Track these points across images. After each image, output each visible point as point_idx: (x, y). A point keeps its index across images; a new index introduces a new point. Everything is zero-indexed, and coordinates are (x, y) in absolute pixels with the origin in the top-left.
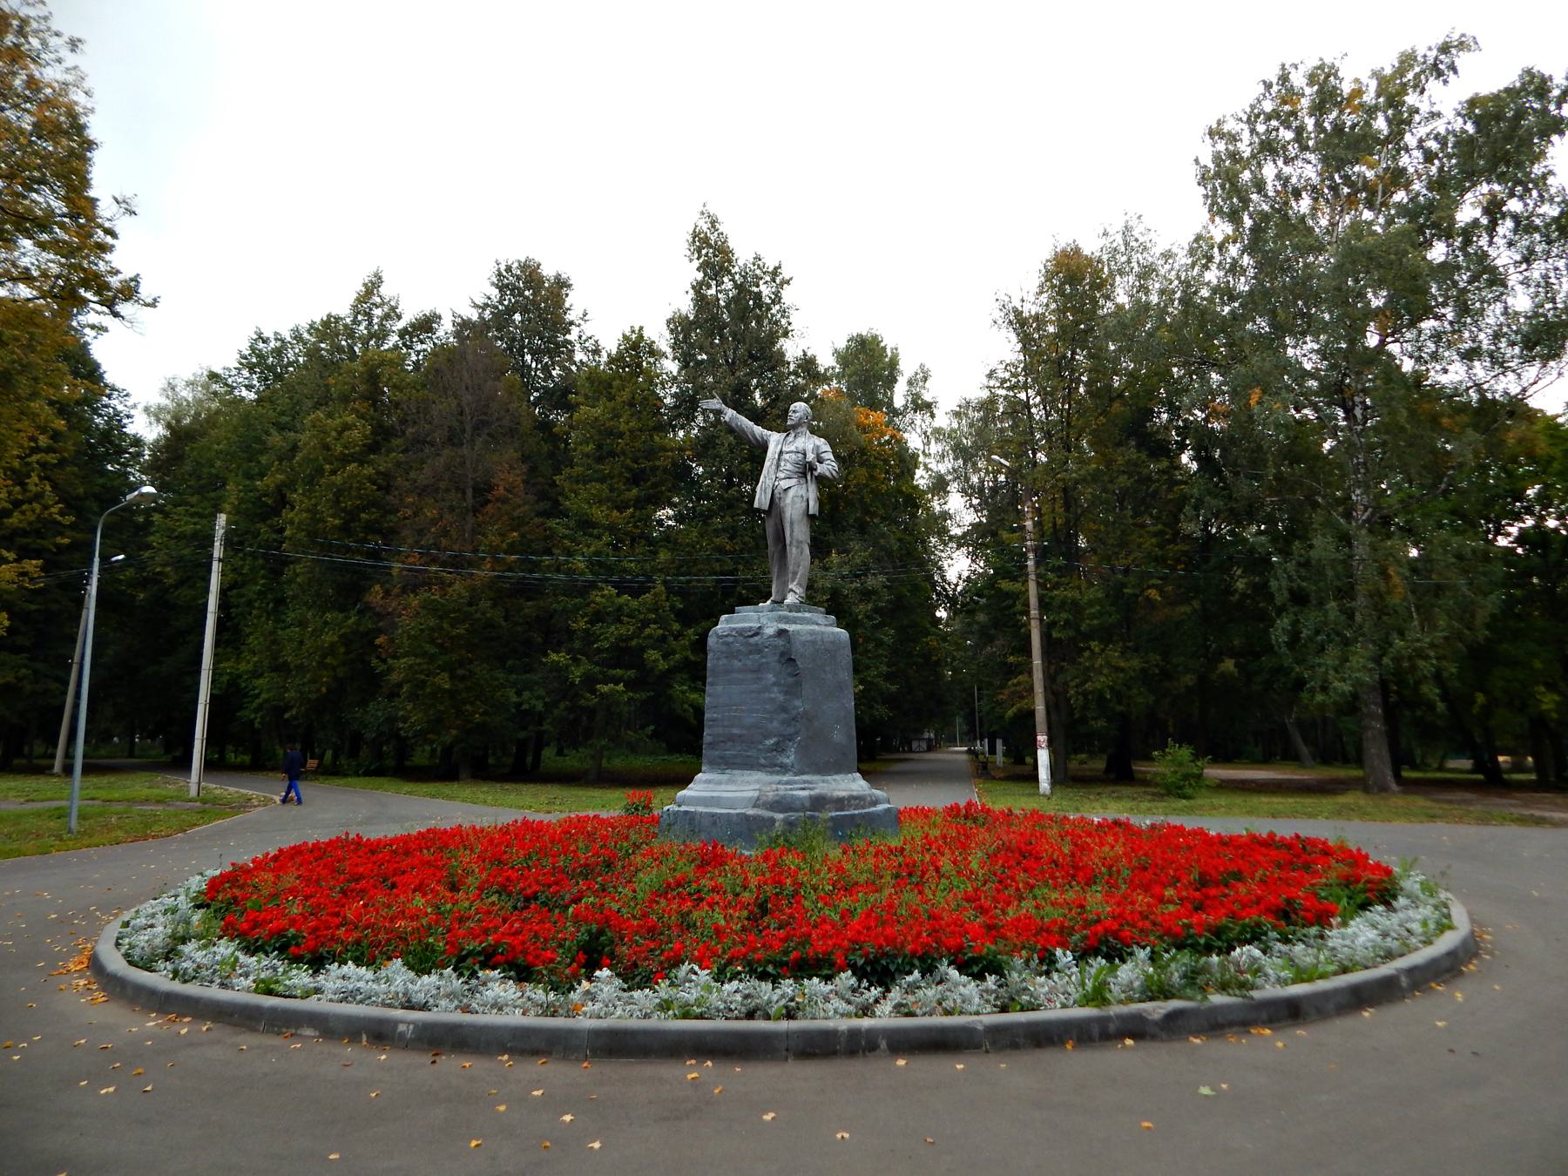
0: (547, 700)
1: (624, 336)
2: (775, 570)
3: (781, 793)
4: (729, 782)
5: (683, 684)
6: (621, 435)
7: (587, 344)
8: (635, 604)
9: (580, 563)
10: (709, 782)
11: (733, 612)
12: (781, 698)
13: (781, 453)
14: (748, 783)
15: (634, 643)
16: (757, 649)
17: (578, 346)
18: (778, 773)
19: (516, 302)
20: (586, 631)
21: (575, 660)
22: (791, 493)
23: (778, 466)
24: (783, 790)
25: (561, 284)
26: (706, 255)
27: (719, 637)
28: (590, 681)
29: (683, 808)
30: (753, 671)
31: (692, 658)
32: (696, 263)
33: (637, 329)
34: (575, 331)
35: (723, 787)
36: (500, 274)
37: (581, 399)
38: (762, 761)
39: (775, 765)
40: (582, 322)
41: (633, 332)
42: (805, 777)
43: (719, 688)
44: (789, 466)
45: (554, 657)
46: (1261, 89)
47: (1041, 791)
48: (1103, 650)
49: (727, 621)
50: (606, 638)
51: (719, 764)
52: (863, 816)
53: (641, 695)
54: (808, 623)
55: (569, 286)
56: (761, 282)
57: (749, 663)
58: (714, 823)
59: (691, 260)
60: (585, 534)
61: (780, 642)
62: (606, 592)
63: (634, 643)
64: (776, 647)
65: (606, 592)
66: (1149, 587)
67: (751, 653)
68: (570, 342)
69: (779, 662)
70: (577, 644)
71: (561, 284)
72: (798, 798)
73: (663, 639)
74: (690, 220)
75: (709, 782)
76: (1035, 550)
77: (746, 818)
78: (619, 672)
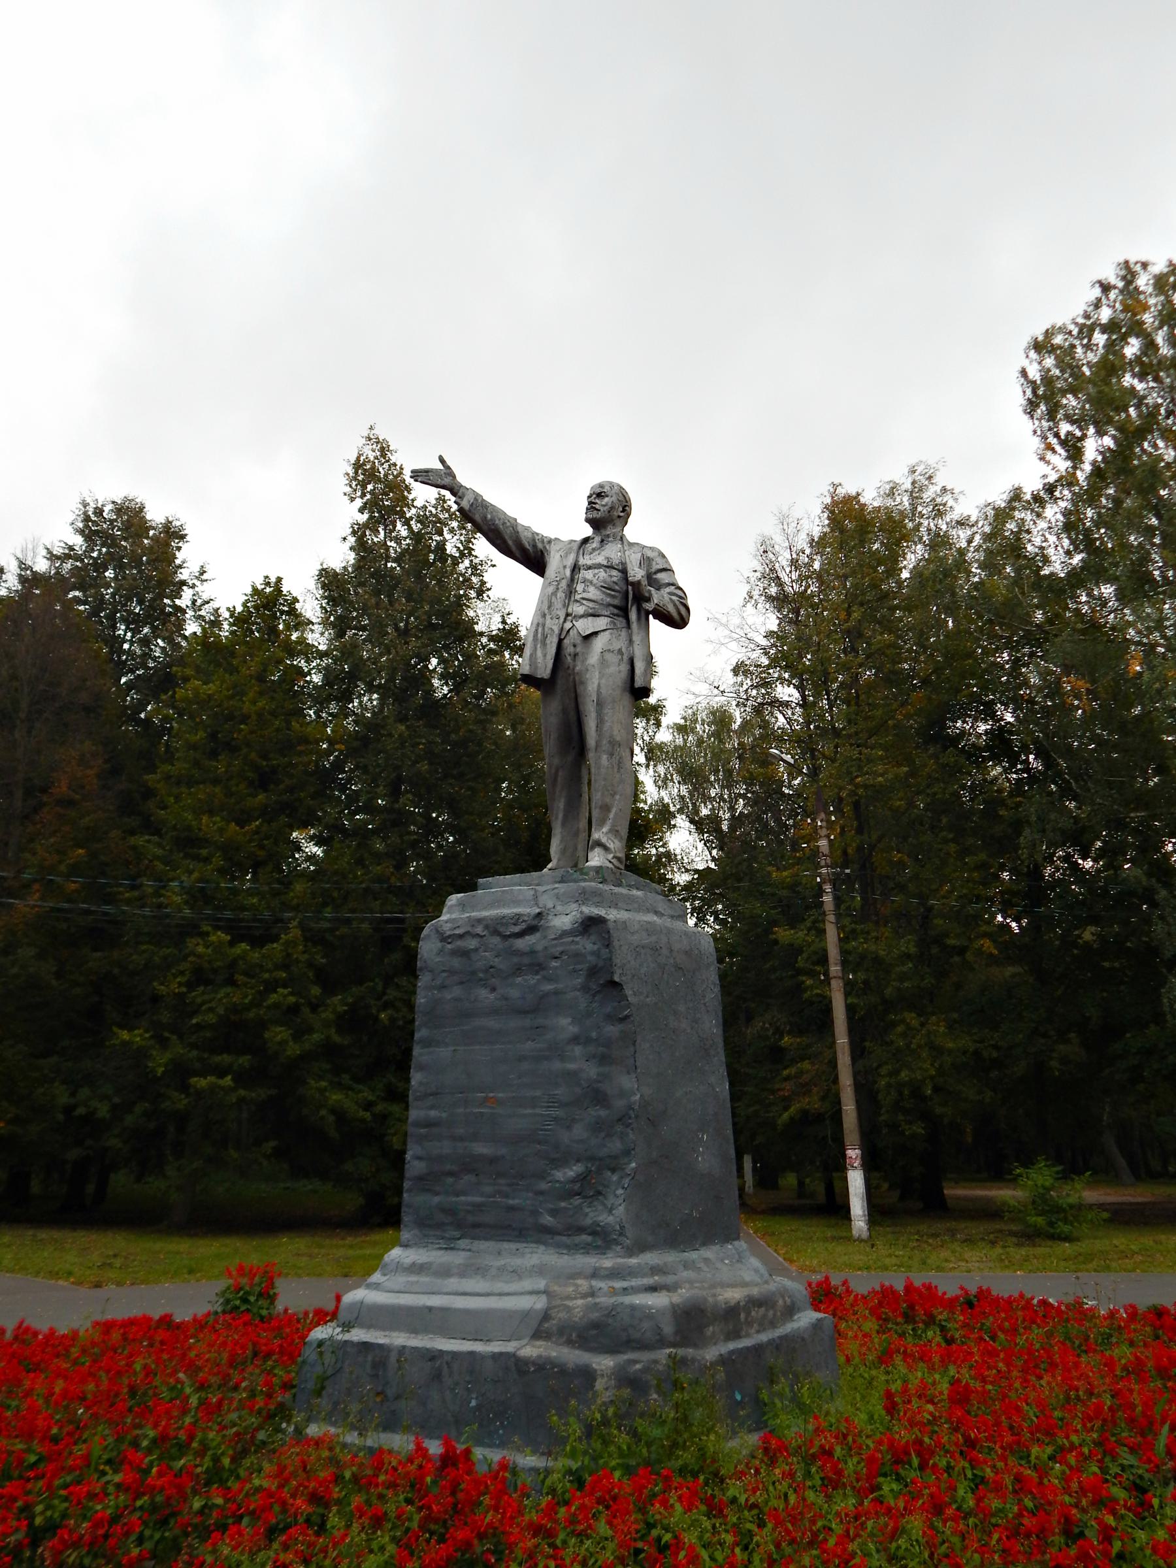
0: (116, 1100)
1: (255, 590)
2: (560, 805)
3: (602, 1300)
4: (480, 1271)
5: (321, 1078)
6: (245, 719)
7: (202, 613)
8: (255, 956)
9: (175, 897)
10: (416, 1269)
11: (473, 887)
12: (592, 1071)
13: (576, 568)
14: (518, 1274)
15: (251, 1015)
16: (535, 964)
17: (190, 613)
18: (587, 1249)
19: (108, 553)
20: (181, 996)
21: (163, 1043)
22: (599, 644)
23: (570, 592)
24: (607, 1293)
25: (172, 534)
26: (372, 492)
27: (444, 939)
28: (180, 1073)
29: (358, 1335)
30: (523, 1012)
31: (337, 1039)
32: (359, 503)
33: (273, 580)
34: (187, 596)
35: (453, 1283)
36: (87, 519)
37: (189, 672)
38: (547, 1220)
39: (581, 1230)
40: (197, 583)
41: (268, 584)
42: (650, 1258)
43: (444, 1053)
44: (593, 593)
45: (125, 1035)
46: (1097, 292)
47: (855, 1233)
48: (922, 1025)
49: (462, 905)
50: (211, 1010)
51: (440, 1226)
52: (777, 1345)
53: (261, 1093)
54: (639, 910)
55: (182, 537)
56: (445, 530)
57: (514, 993)
58: (437, 1376)
59: (352, 500)
60: (187, 856)
61: (587, 945)
62: (213, 938)
63: (251, 1015)
64: (577, 956)
65: (213, 938)
66: (978, 937)
67: (518, 970)
68: (179, 609)
69: (585, 988)
70: (165, 1017)
71: (172, 534)
72: (646, 1314)
73: (294, 1010)
74: (351, 447)
75: (416, 1269)
76: (835, 881)
77: (518, 1365)
78: (225, 1059)
